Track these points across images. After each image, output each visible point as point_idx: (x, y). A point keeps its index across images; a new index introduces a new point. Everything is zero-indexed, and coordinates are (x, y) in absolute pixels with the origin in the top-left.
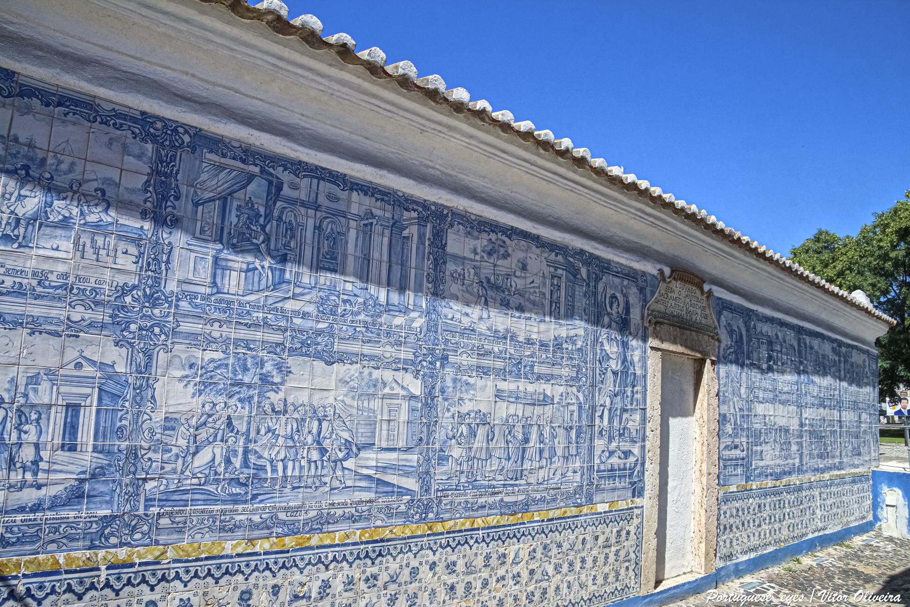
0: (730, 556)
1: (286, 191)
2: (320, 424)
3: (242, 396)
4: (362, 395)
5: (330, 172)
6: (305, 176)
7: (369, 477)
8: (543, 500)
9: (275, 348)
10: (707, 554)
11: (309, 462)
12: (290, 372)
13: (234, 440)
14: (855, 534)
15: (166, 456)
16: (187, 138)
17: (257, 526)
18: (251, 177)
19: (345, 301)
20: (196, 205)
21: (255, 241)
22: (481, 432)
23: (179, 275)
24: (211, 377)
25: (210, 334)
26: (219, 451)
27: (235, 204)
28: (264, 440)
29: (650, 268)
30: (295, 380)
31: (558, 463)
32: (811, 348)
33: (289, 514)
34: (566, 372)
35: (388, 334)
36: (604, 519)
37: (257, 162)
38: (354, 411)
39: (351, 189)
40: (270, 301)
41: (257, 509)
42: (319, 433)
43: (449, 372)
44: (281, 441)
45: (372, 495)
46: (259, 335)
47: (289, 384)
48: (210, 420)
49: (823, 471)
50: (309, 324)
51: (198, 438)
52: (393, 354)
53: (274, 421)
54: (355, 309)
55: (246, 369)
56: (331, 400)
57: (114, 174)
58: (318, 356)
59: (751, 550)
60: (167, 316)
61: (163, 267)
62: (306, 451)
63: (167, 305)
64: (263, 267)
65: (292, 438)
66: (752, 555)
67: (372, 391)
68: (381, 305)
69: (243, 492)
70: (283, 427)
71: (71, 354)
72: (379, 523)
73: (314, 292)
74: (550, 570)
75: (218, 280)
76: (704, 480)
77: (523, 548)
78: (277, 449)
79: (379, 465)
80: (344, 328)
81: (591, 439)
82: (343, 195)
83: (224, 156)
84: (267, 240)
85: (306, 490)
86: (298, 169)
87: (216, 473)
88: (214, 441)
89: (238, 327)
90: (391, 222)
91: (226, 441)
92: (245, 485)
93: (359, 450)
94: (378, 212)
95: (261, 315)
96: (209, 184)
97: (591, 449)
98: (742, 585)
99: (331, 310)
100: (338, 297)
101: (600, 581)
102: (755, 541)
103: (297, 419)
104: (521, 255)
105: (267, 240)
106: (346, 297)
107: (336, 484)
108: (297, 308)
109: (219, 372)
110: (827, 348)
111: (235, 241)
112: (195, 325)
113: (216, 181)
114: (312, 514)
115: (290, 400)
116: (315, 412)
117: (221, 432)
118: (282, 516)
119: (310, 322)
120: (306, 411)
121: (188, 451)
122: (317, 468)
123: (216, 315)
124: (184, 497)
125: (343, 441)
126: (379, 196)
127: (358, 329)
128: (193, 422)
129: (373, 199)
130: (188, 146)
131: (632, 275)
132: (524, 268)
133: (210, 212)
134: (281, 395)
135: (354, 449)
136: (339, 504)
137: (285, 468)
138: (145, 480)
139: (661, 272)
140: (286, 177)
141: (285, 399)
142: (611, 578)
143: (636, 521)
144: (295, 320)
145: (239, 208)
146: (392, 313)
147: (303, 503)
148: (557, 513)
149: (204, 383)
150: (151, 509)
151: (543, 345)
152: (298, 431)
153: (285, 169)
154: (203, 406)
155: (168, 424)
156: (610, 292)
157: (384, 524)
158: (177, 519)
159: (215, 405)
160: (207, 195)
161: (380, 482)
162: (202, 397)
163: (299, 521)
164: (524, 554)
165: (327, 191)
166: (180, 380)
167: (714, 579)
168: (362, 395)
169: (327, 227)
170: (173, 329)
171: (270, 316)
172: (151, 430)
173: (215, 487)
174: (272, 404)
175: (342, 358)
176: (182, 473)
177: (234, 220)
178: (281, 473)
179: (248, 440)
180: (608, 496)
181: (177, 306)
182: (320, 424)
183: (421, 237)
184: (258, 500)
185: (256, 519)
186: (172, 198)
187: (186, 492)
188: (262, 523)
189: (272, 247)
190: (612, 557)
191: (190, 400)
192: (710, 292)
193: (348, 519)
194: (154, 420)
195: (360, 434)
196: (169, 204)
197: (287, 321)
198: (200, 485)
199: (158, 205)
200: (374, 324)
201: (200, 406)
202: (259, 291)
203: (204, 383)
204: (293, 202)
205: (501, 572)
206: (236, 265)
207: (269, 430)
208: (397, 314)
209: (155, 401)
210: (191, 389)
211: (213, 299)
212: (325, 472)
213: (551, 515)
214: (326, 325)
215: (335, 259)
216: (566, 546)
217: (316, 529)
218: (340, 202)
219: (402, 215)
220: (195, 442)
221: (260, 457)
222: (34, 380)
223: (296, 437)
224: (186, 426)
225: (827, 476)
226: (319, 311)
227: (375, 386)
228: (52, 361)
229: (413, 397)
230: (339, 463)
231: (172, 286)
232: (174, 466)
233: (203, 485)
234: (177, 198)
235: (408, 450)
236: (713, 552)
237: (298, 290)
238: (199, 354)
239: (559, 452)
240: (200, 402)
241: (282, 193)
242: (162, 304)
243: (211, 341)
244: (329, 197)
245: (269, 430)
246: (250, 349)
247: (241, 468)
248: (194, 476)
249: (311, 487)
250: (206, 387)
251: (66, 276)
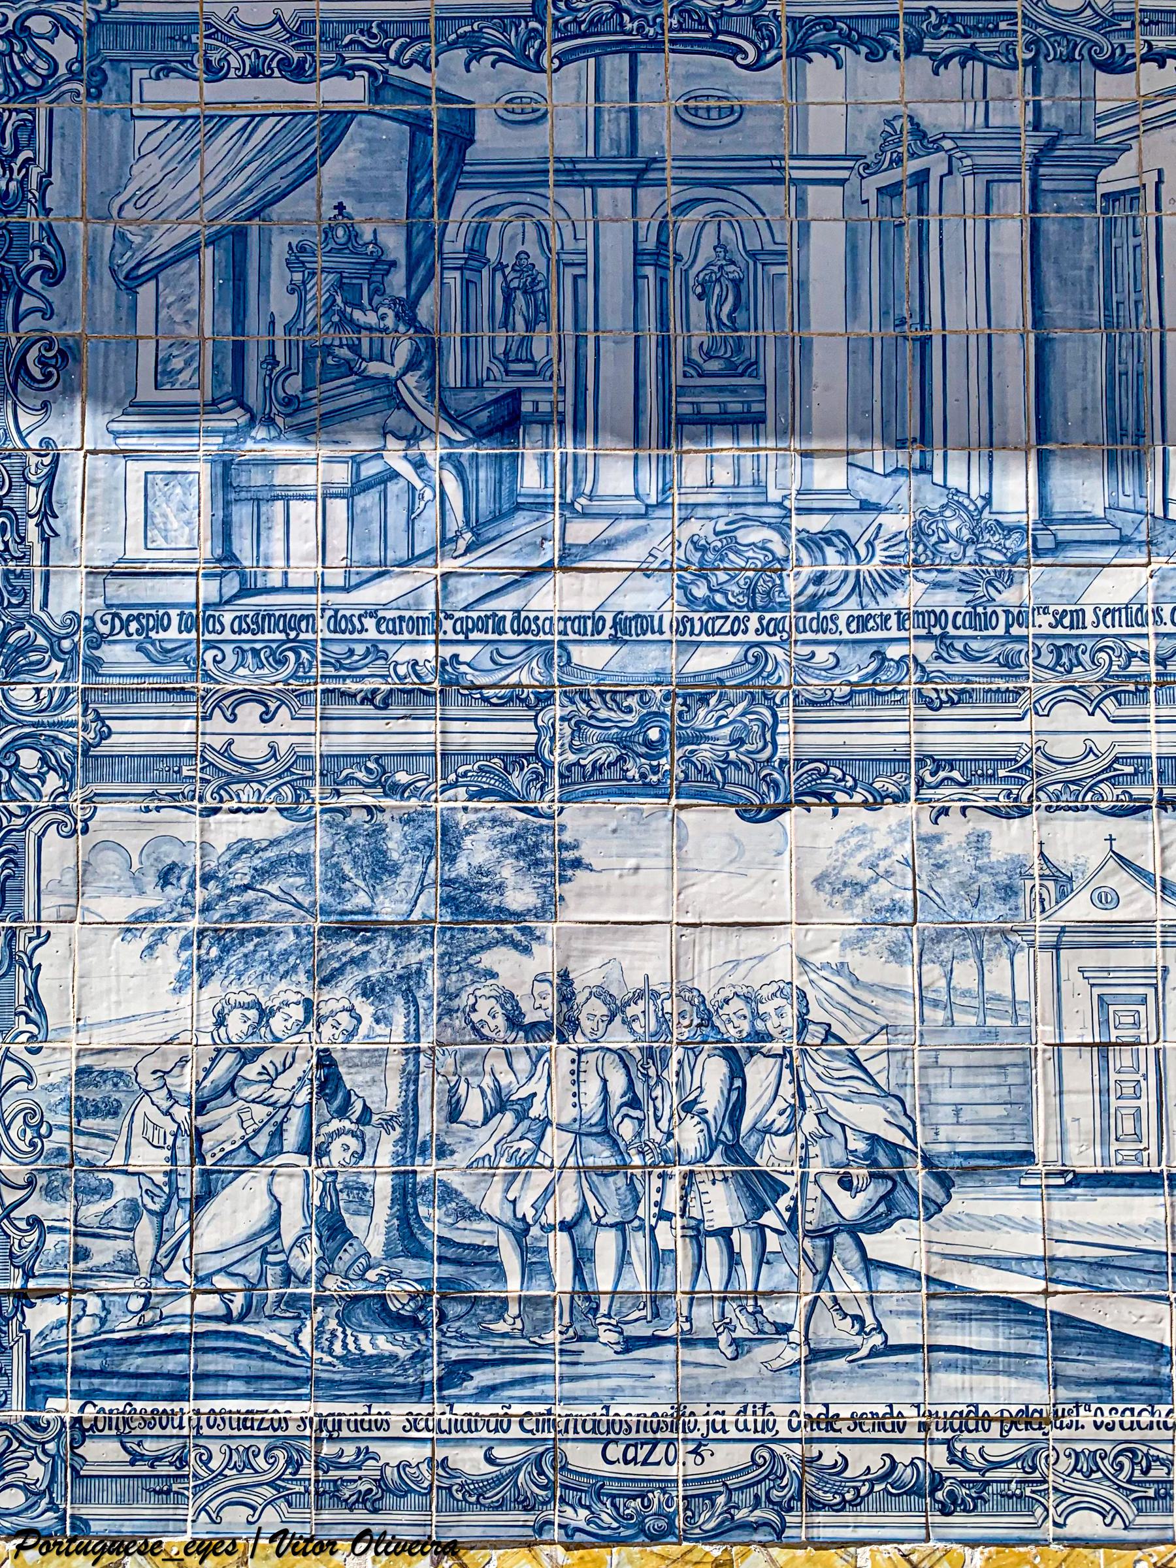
1: (492, 140)
2: (737, 1071)
3: (374, 972)
4: (939, 937)
6: (564, 59)
9: (497, 775)
11: (697, 1233)
12: (577, 863)
13: (354, 1144)
15: (92, 1211)
16: (64, 49)
17: (476, 1494)
18: (335, 126)
19: (813, 543)
20: (130, 282)
21: (375, 368)
22: (794, 1425)
23: (97, 550)
24: (246, 911)
25: (226, 752)
26: (293, 1188)
27: (280, 246)
28: (485, 1142)
30: (603, 893)
33: (614, 1452)
35: (1064, 655)
37: (353, 57)
38: (907, 1011)
39: (800, 52)
40: (465, 592)
41: (472, 1422)
42: (735, 1110)
44: (556, 1144)
45: (1034, 1393)
46: (423, 733)
47: (574, 912)
48: (251, 1071)
50: (646, 660)
51: (208, 1141)
52: (1102, 743)
53: (522, 1063)
54: (875, 566)
55: (381, 868)
56: (781, 967)
58: (706, 787)
60: (62, 705)
61: (33, 534)
62: (674, 1188)
63: (57, 666)
64: (419, 465)
65: (607, 1133)
67: (992, 913)
68: (1009, 530)
69: (404, 1354)
70: (563, 1089)
72: (1086, 1524)
73: (660, 528)
75: (243, 547)
78: (540, 1179)
79: (1061, 1251)
80: (823, 654)
82: (760, 89)
83: (215, 73)
84: (428, 354)
85: (686, 1354)
86: (533, 34)
87: (288, 1275)
88: (271, 1153)
89: (334, 710)
90: (1029, 145)
91: (323, 1152)
92: (413, 1323)
93: (945, 1182)
95: (429, 651)
96: (171, 193)
99: (751, 590)
100: (781, 528)
103: (622, 1056)
105: (428, 354)
106: (817, 524)
107: (833, 1330)
108: (589, 605)
109: (273, 888)
111: (294, 385)
112: (168, 725)
113: (195, 176)
114: (727, 1457)
115: (586, 976)
116: (707, 1020)
117: (296, 1116)
118: (584, 1457)
119: (654, 652)
120: (663, 1020)
121: (175, 1190)
122: (733, 1259)
123: (245, 678)
124: (173, 1363)
125: (861, 1146)
126: (947, 45)
127: (894, 652)
128: (185, 1082)
129: (922, 64)
130: (73, 76)
133: (184, 299)
134: (543, 959)
135: (920, 1178)
136: (857, 1421)
137: (582, 1259)
138: (23, 1297)
140: (482, 84)
141: (565, 976)
144: (580, 655)
145: (298, 257)
146: (1075, 555)
147: (679, 1409)
149: (218, 936)
150: (52, 1403)
152: (634, 1103)
153: (477, 55)
154: (221, 1021)
155: (92, 1095)
157: (1117, 1531)
158: (150, 1446)
159: (265, 1014)
160: (165, 240)
161: (1071, 1332)
162: (214, 987)
163: (665, 1484)
165: (676, 88)
166: (130, 927)
168: (939, 937)
169: (698, 241)
170: (87, 747)
171: (467, 653)
172: (31, 1113)
173: (287, 1327)
174: (508, 999)
175: (818, 786)
176: (158, 1272)
177: (282, 305)
178: (564, 1279)
179: (413, 1145)
181: (94, 665)
182: (737, 1071)
184: (470, 1387)
185: (470, 1461)
186: (35, 282)
187: (176, 1344)
188: (498, 1480)
189: (453, 378)
191: (170, 1002)
193: (916, 1491)
194: (41, 1081)
195: (944, 1114)
196: (28, 302)
197: (548, 663)
198: (228, 1318)
200: (979, 619)
201: (209, 1022)
202: (413, 559)
203: (218, 936)
204: (522, 177)
206: (308, 477)
207: (500, 1103)
208: (1106, 554)
209: (42, 1012)
210: (170, 960)
211: (227, 618)
212: (775, 1277)
214: (731, 654)
215: (752, 367)
217: (755, 1527)
218: (749, 120)
219: (1088, 98)
220: (198, 1155)
221: (473, 1213)
223: (627, 1130)
224: (160, 1096)
226: (692, 601)
227: (1008, 892)
230: (843, 1239)
231: (70, 596)
232: (123, 1246)
233: (240, 1320)
234: (54, 276)
237: (582, 532)
238: (188, 827)
240: (207, 1006)
241: (470, 154)
242: (41, 666)
244: (691, 114)
245: (500, 1103)
246: (394, 790)
247: (389, 1254)
248: (202, 1283)
249: (712, 1343)
250: (226, 950)
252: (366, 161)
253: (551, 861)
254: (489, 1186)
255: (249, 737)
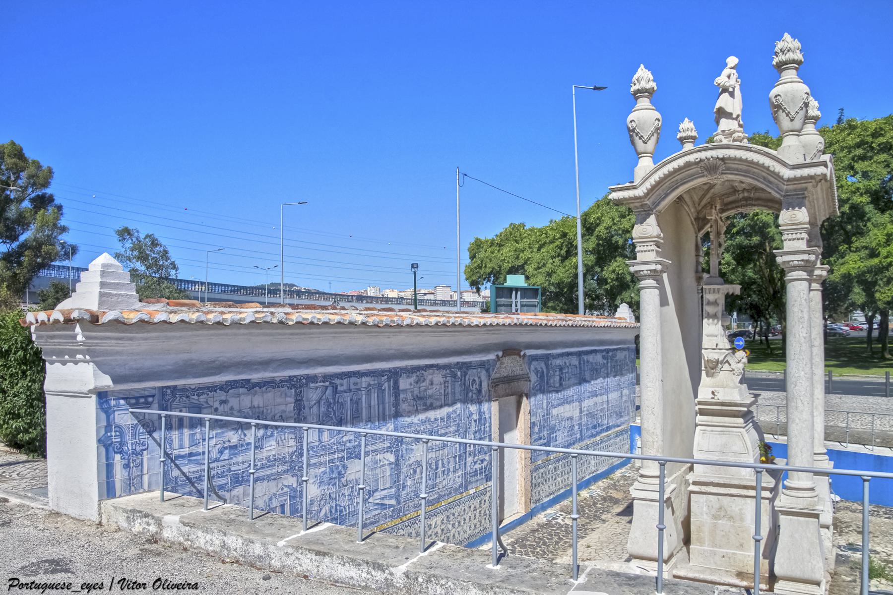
0: (539, 500)
1: (339, 388)
5: (353, 372)
7: (378, 504)
8: (445, 495)
9: (341, 459)
10: (526, 502)
14: (617, 469)
18: (327, 387)
29: (492, 357)
31: (451, 475)
32: (588, 362)
34: (452, 429)
36: (473, 497)
43: (404, 446)
49: (595, 436)
55: (333, 472)
57: (283, 407)
59: (550, 494)
66: (551, 497)
71: (280, 485)
74: (450, 527)
76: (523, 462)
77: (438, 519)
81: (466, 459)
94: (372, 383)
97: (466, 464)
98: (546, 516)
101: (473, 527)
102: (553, 489)
104: (430, 377)
110: (599, 358)
131: (482, 365)
132: (432, 384)
139: (497, 356)
140: (338, 381)
142: (478, 526)
143: (488, 494)
148: (452, 499)
151: (442, 419)
156: (472, 378)
161: (382, 505)
164: (439, 523)
167: (530, 515)
180: (474, 485)
183: (389, 387)
190: (478, 515)
192: (525, 355)
199: (299, 414)
205: (430, 533)
213: (449, 501)
216: (456, 514)
222: (270, 499)
225: (598, 438)
228: (274, 491)
229: (391, 463)
235: (391, 488)
236: (528, 500)
238: (317, 471)
239: (452, 470)
243: (321, 464)
251: (275, 455)
252: (329, 391)
253: (345, 467)
254: (344, 502)
255: (322, 459)
